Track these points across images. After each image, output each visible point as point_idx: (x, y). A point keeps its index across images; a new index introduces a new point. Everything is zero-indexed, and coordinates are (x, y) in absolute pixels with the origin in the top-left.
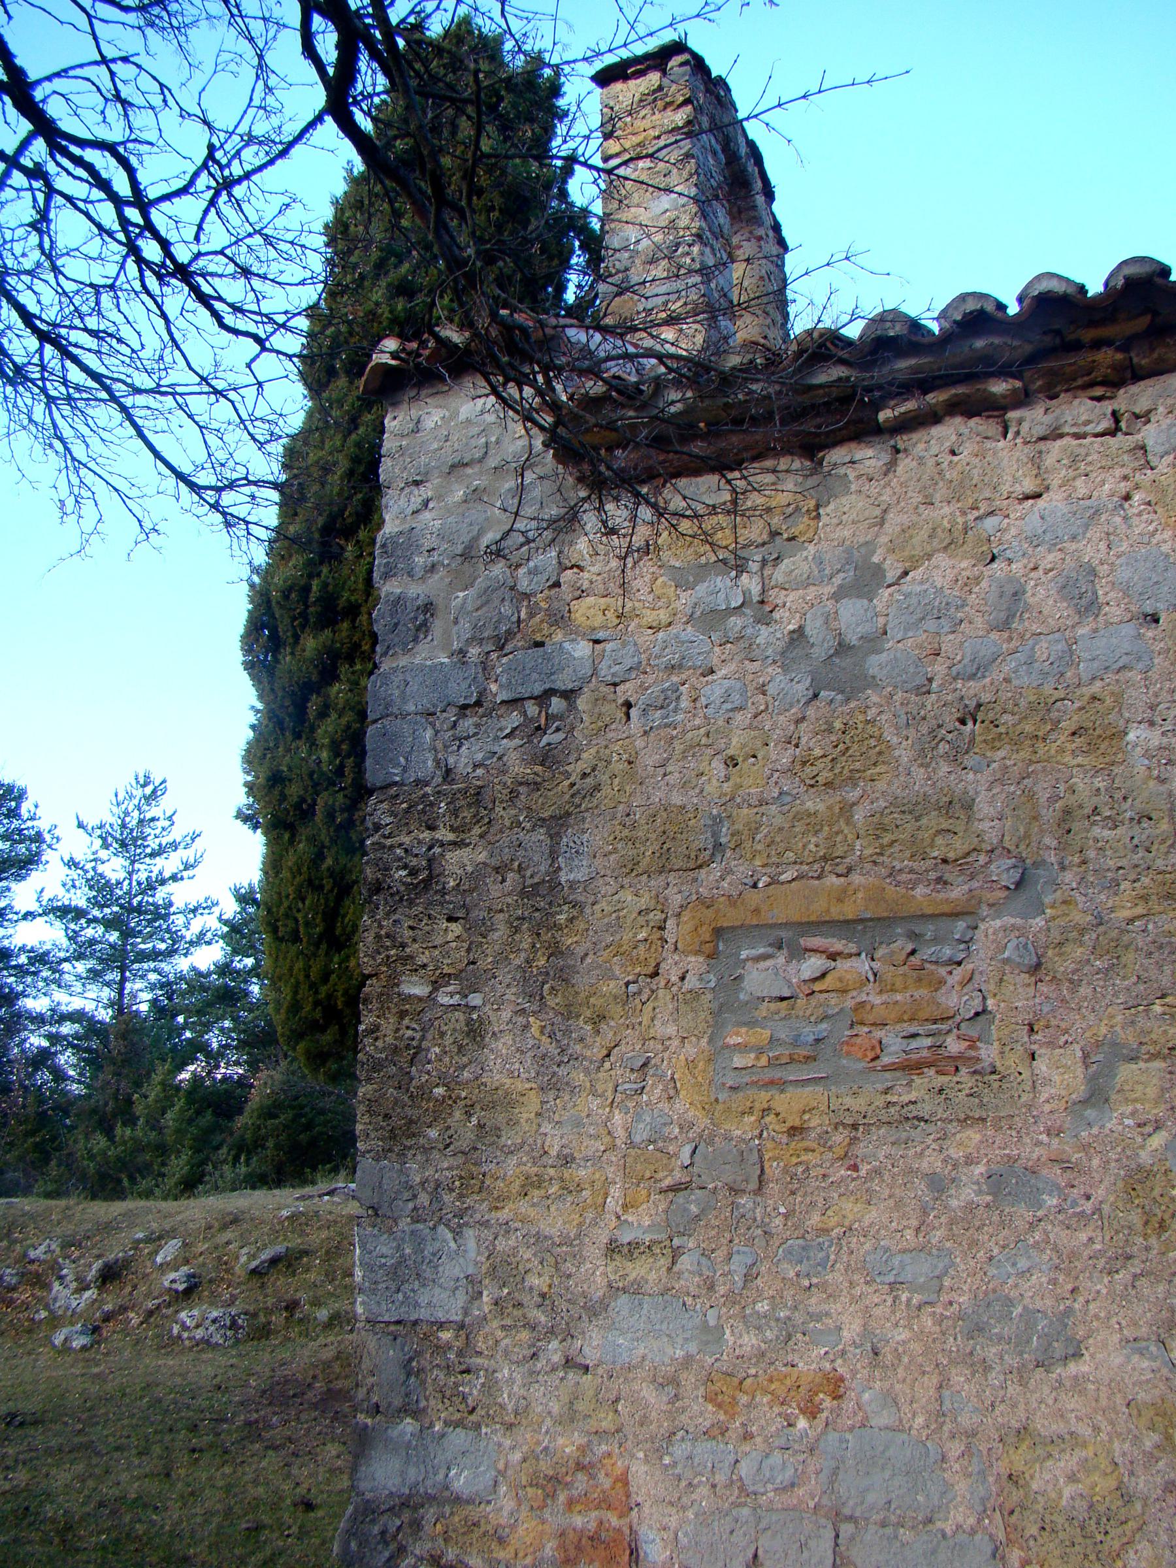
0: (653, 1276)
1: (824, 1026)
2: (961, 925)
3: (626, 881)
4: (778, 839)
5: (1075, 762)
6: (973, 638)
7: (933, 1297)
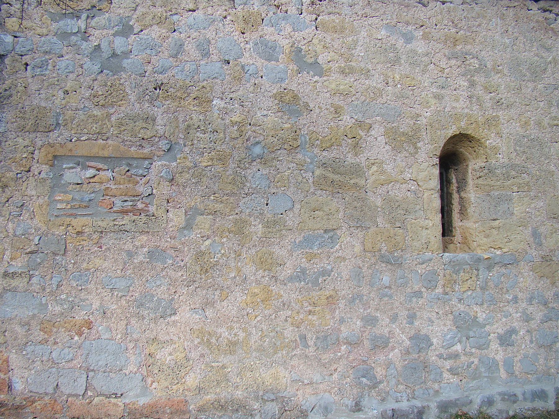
0: (21, 285)
1: (93, 195)
2: (147, 162)
3: (20, 134)
4: (81, 124)
5: (194, 109)
6: (162, 59)
7: (126, 294)
